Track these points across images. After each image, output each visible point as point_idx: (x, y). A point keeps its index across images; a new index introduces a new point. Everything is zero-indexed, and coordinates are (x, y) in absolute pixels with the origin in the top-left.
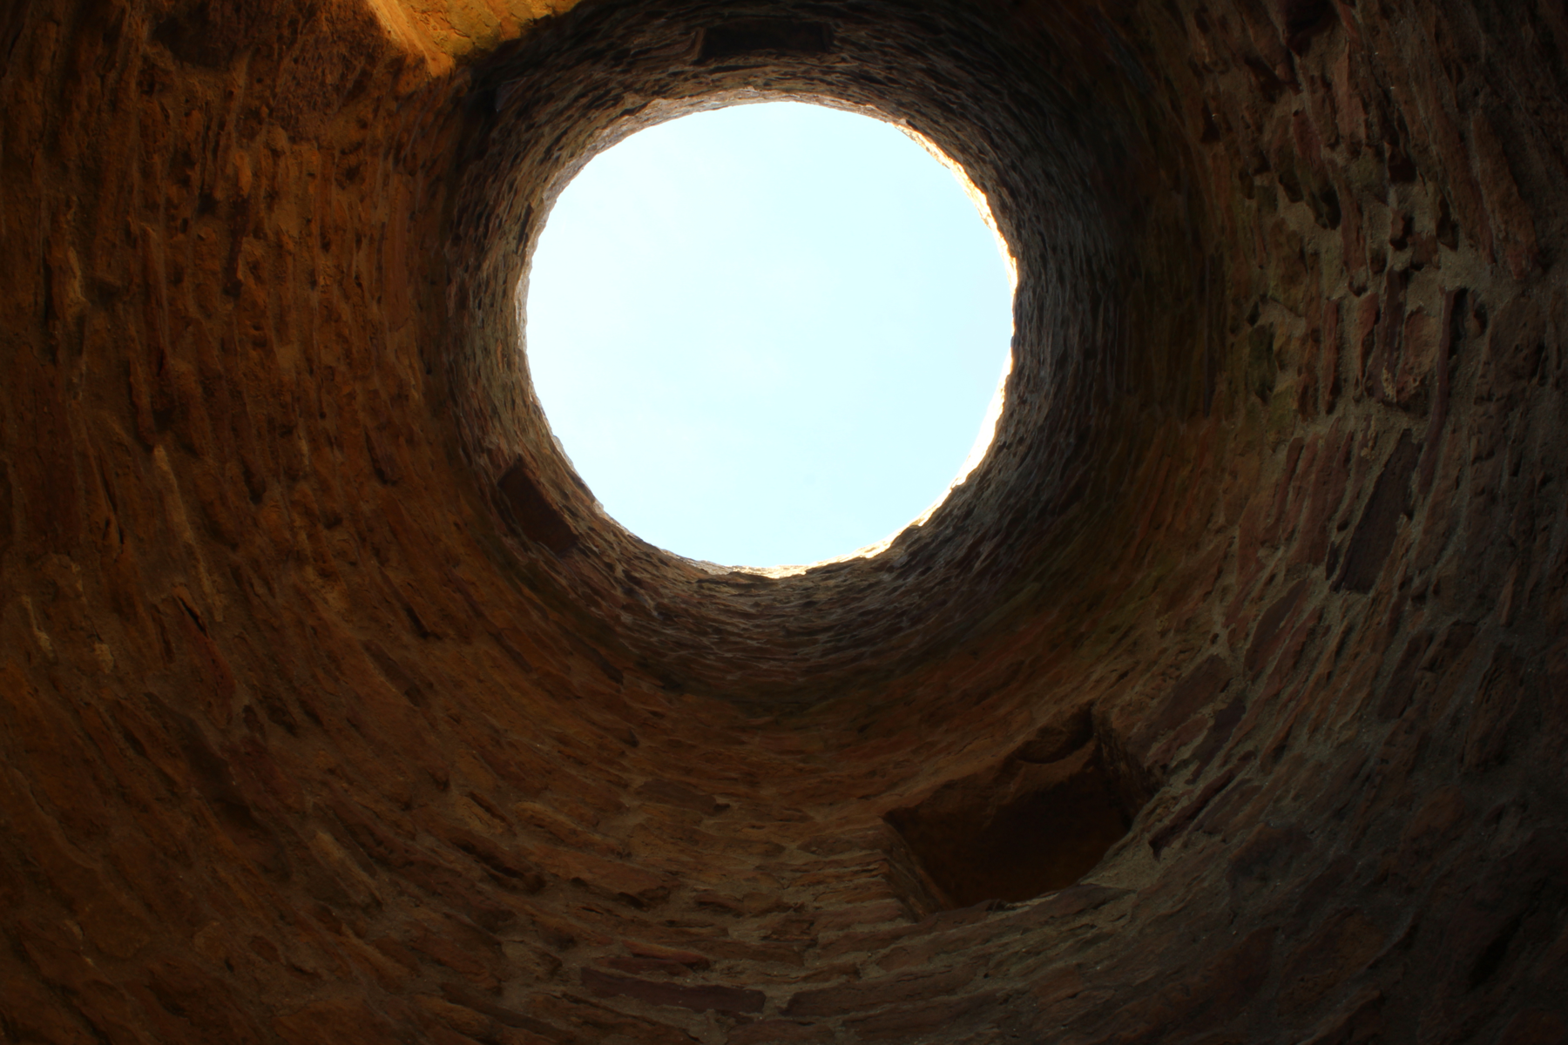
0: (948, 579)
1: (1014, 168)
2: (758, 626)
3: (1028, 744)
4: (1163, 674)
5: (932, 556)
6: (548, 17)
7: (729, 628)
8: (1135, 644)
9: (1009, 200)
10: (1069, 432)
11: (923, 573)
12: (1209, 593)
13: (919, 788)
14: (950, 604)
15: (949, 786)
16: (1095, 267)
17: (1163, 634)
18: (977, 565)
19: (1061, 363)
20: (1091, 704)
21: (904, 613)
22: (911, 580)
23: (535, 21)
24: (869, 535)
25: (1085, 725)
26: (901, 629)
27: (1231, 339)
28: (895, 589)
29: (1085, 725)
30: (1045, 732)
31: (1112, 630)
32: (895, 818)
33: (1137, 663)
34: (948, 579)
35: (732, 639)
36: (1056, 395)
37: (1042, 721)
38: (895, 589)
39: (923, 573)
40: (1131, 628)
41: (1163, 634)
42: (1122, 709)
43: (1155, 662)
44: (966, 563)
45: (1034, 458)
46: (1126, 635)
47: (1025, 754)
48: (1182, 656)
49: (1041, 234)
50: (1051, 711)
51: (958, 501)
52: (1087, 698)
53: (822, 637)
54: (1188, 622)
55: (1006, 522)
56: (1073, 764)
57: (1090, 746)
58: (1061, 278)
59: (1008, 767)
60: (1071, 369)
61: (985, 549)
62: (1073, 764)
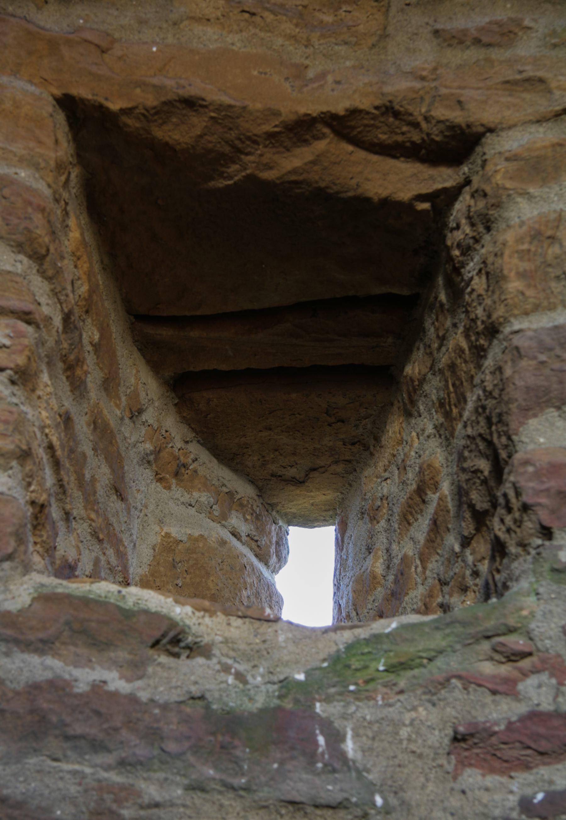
15: (191, 104)
47: (343, 125)
56: (403, 181)
59: (302, 129)
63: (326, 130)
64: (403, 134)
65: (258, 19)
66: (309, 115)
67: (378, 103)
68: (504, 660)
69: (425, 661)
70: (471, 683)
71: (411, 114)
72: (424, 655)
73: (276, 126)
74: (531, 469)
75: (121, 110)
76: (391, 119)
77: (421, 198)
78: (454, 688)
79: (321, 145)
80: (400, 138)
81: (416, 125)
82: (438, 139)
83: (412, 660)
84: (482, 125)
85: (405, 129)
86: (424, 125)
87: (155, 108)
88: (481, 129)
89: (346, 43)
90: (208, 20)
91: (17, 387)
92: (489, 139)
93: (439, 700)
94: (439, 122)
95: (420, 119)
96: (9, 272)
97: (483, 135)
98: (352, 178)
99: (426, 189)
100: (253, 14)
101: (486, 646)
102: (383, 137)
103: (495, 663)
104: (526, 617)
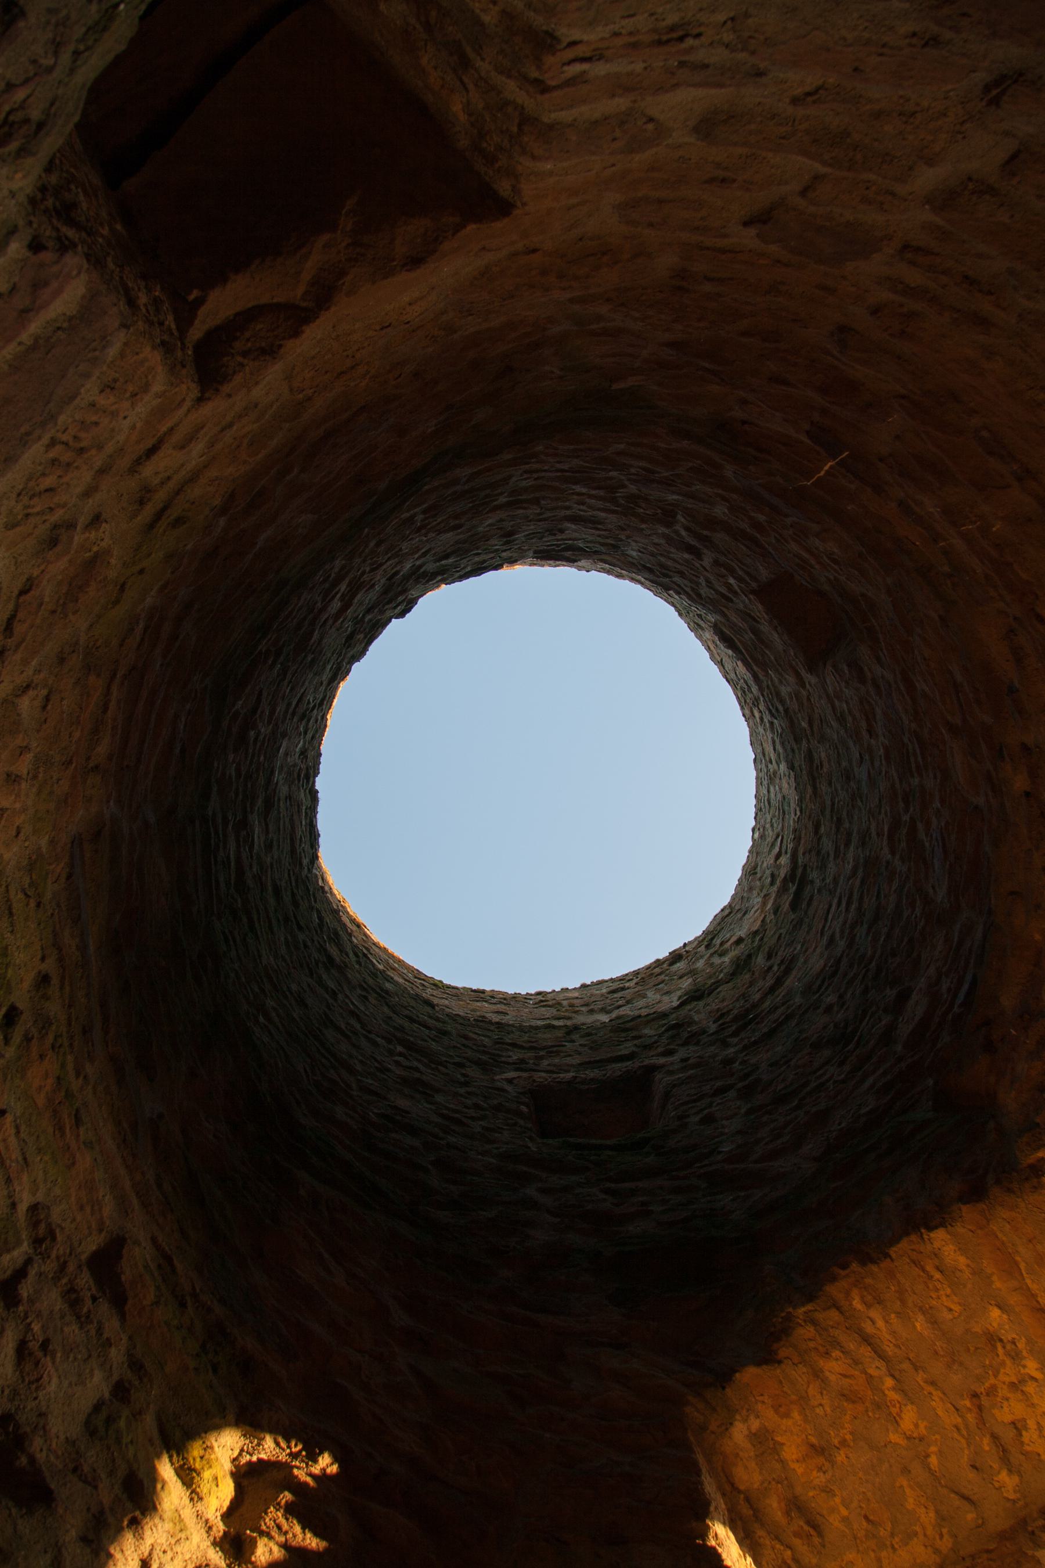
0: (372, 570)
1: (334, 994)
2: (568, 508)
3: (296, 333)
4: (82, 451)
5: (385, 591)
6: (930, 1229)
7: (600, 504)
8: (142, 502)
9: (333, 951)
10: (256, 739)
11: (396, 573)
12: (23, 592)
13: (463, 261)
14: (372, 544)
15: (415, 261)
16: (245, 919)
17: (96, 520)
18: (343, 587)
19: (269, 804)
20: (200, 400)
21: (419, 529)
22: (408, 566)
23: (942, 1225)
24: (441, 606)
25: (209, 365)
26: (424, 512)
27: (50, 966)
28: (425, 554)
29: (209, 365)
30: (270, 352)
31: (179, 521)
32: (490, 205)
33: (133, 470)
34: (372, 570)
35: (602, 493)
36: (272, 772)
37: (274, 372)
38: (425, 554)
39: (396, 573)
40: (152, 526)
41: (96, 520)
42: (146, 388)
43: (102, 471)
44: (356, 587)
45: (289, 704)
46: (159, 516)
47: (297, 317)
48: (48, 482)
49: (300, 928)
50: (265, 387)
51: (359, 647)
52: (207, 409)
53: (502, 500)
54: (53, 542)
55: (316, 635)
56: (222, 303)
57: (196, 333)
58: (277, 891)
59: (323, 294)
60: (260, 803)
61: (336, 605)
62: (222, 303)
63: (304, 304)
64: (248, 340)
65: (378, 328)
66: (326, 310)
67: (282, 350)
68: (11, 118)
69: (82, 47)
70: (36, 75)
71: (254, 360)
72: (86, 54)
73: (344, 284)
74: (75, 273)
75: (465, 227)
76: (263, 344)
77: (200, 302)
78: (46, 53)
79: (301, 290)
80: (247, 334)
81: (245, 354)
82: (225, 359)
83: (96, 40)
84: (209, 399)
85: (249, 344)
86: (240, 359)
87: (441, 243)
88: (207, 395)
89: (313, 358)
90: (410, 304)
91: (544, 28)
92: (195, 393)
93: (48, 23)
94: (234, 372)
95: (246, 361)
96: (562, 109)
97: (203, 392)
98: (261, 280)
99: (202, 311)
100: (382, 329)
101: (36, 115)
102: (259, 327)
103: (16, 106)
104: (16, 172)
